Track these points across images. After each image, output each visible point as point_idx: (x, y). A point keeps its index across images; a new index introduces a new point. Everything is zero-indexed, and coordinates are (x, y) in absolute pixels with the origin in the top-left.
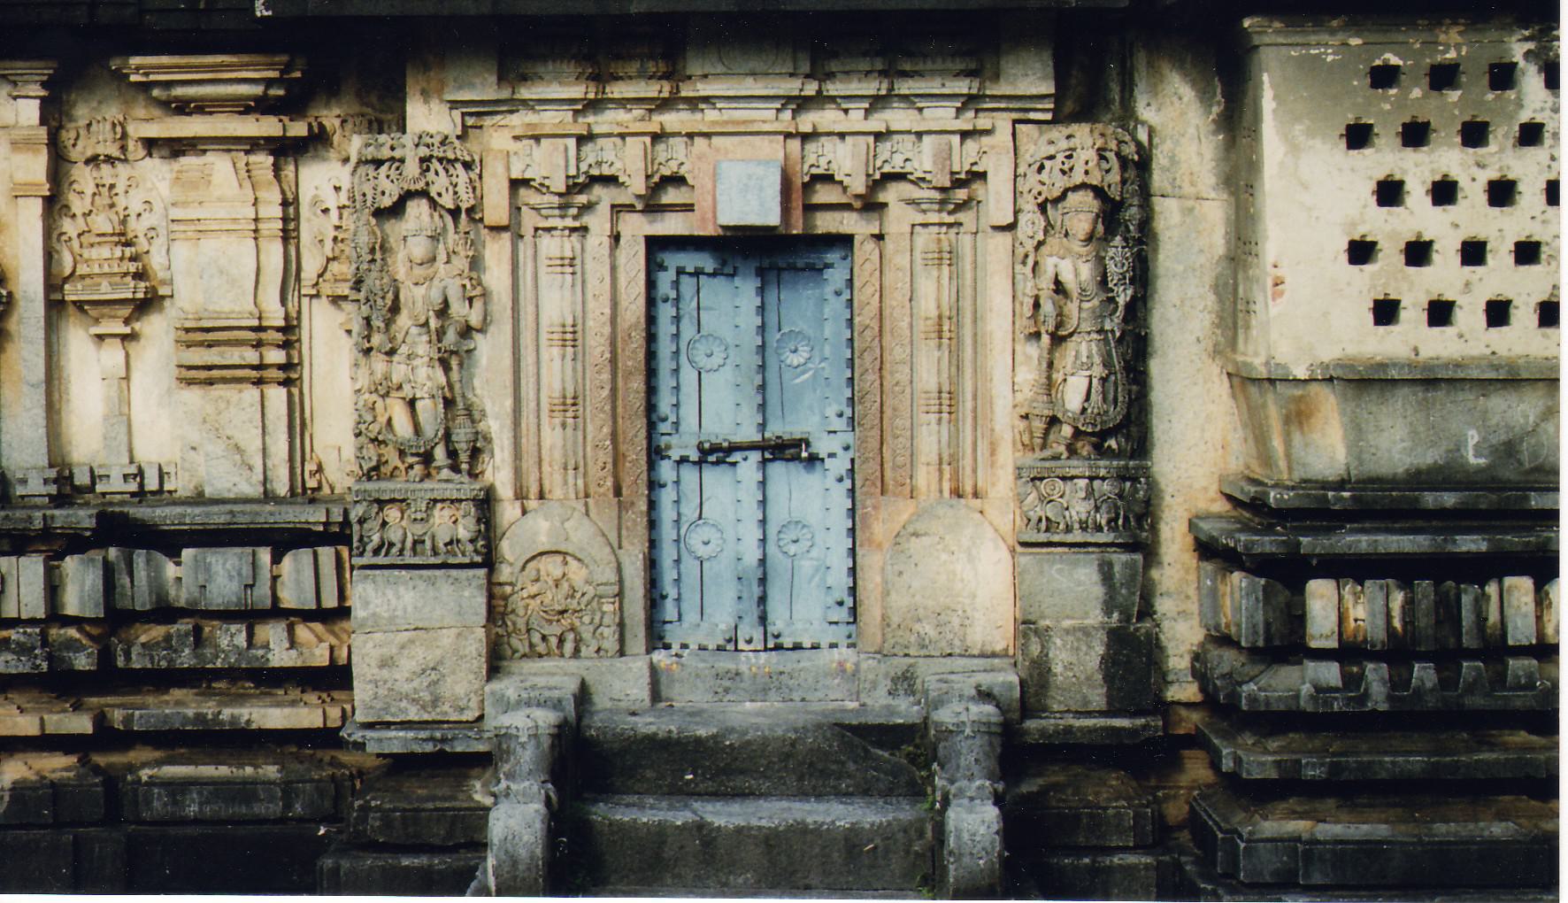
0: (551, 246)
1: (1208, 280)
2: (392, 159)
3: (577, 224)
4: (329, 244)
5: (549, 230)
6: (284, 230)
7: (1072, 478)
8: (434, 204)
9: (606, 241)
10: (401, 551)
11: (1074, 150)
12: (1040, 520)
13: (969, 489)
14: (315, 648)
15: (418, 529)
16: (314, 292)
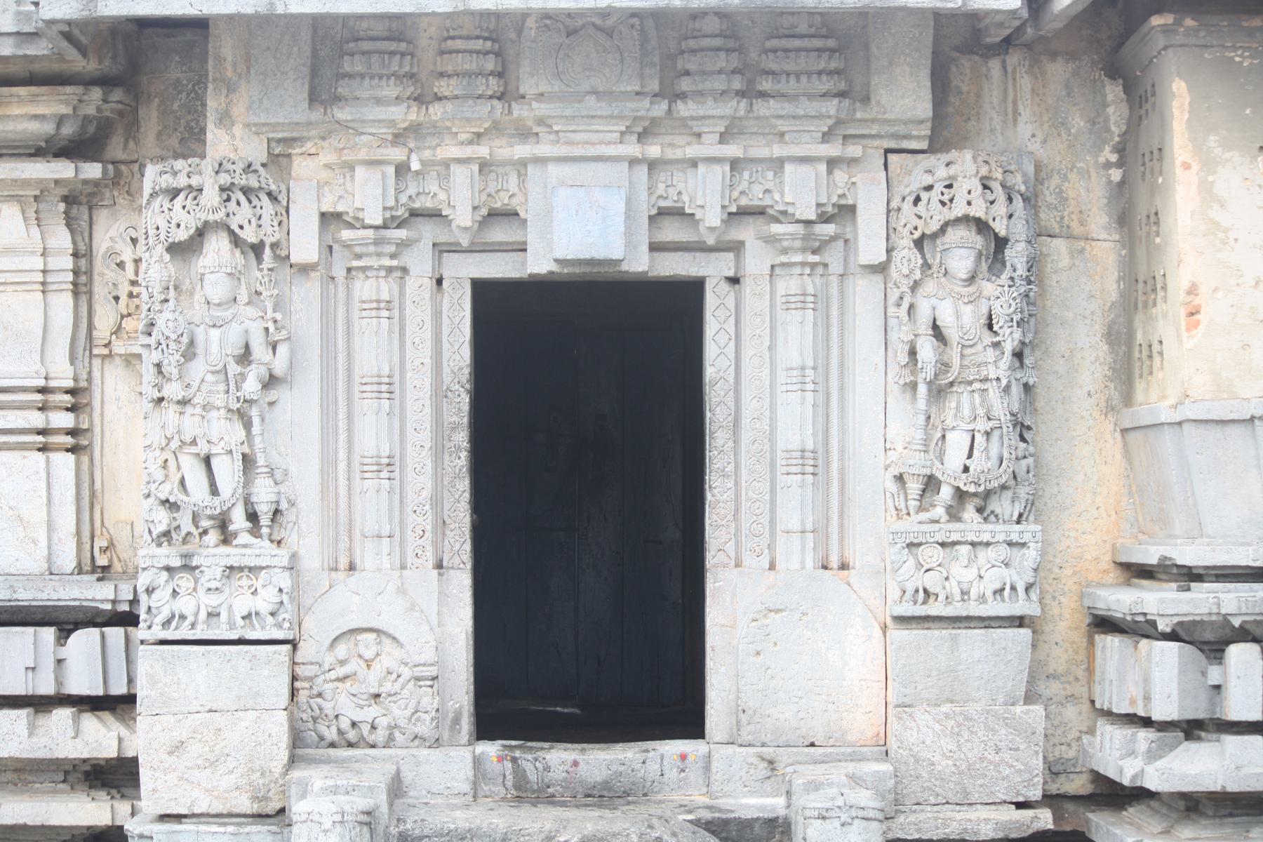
0: (365, 288)
1: (1099, 328)
3: (395, 263)
4: (124, 298)
5: (363, 269)
6: (75, 284)
7: (954, 543)
8: (236, 241)
9: (429, 284)
10: (193, 626)
11: (954, 178)
12: (917, 591)
13: (834, 561)
14: (99, 738)
15: (212, 601)
16: (105, 351)
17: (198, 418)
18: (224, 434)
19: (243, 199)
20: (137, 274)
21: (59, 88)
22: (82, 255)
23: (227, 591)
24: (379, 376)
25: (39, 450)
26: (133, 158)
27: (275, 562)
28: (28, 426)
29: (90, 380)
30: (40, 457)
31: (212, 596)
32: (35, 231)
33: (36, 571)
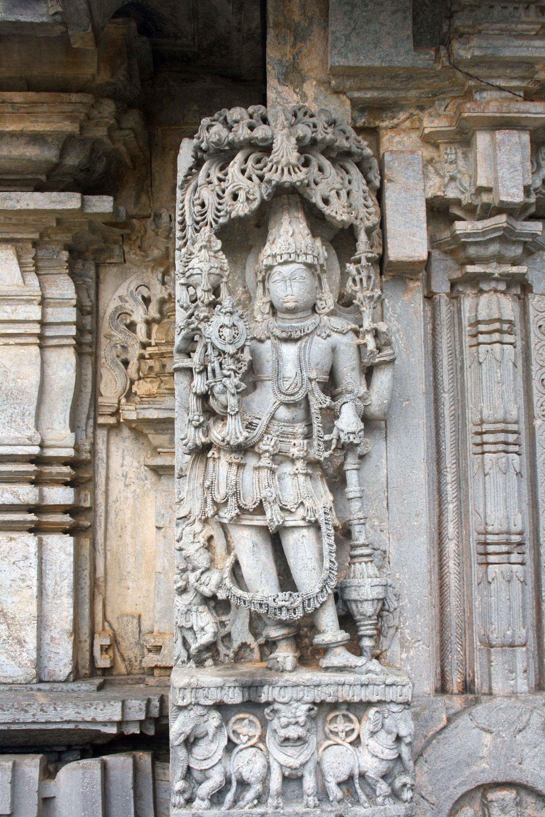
2: (252, 145)
15: (291, 758)
16: (112, 420)
17: (265, 473)
18: (299, 493)
19: (327, 164)
20: (149, 336)
21: (64, 95)
22: (88, 312)
23: (313, 740)
24: (505, 422)
25: (30, 531)
26: (145, 213)
27: (391, 694)
28: (16, 502)
29: (93, 451)
30: (31, 540)
31: (290, 751)
32: (33, 280)
33: (21, 679)
